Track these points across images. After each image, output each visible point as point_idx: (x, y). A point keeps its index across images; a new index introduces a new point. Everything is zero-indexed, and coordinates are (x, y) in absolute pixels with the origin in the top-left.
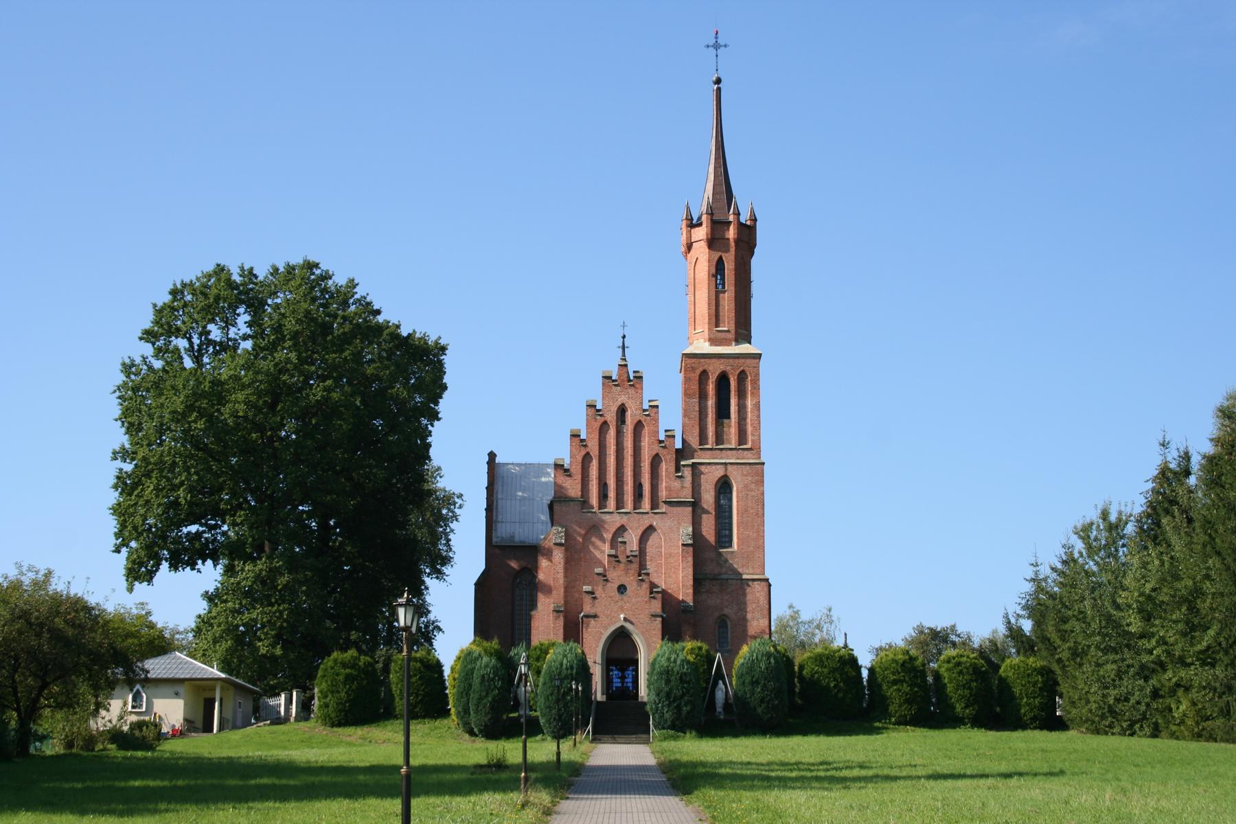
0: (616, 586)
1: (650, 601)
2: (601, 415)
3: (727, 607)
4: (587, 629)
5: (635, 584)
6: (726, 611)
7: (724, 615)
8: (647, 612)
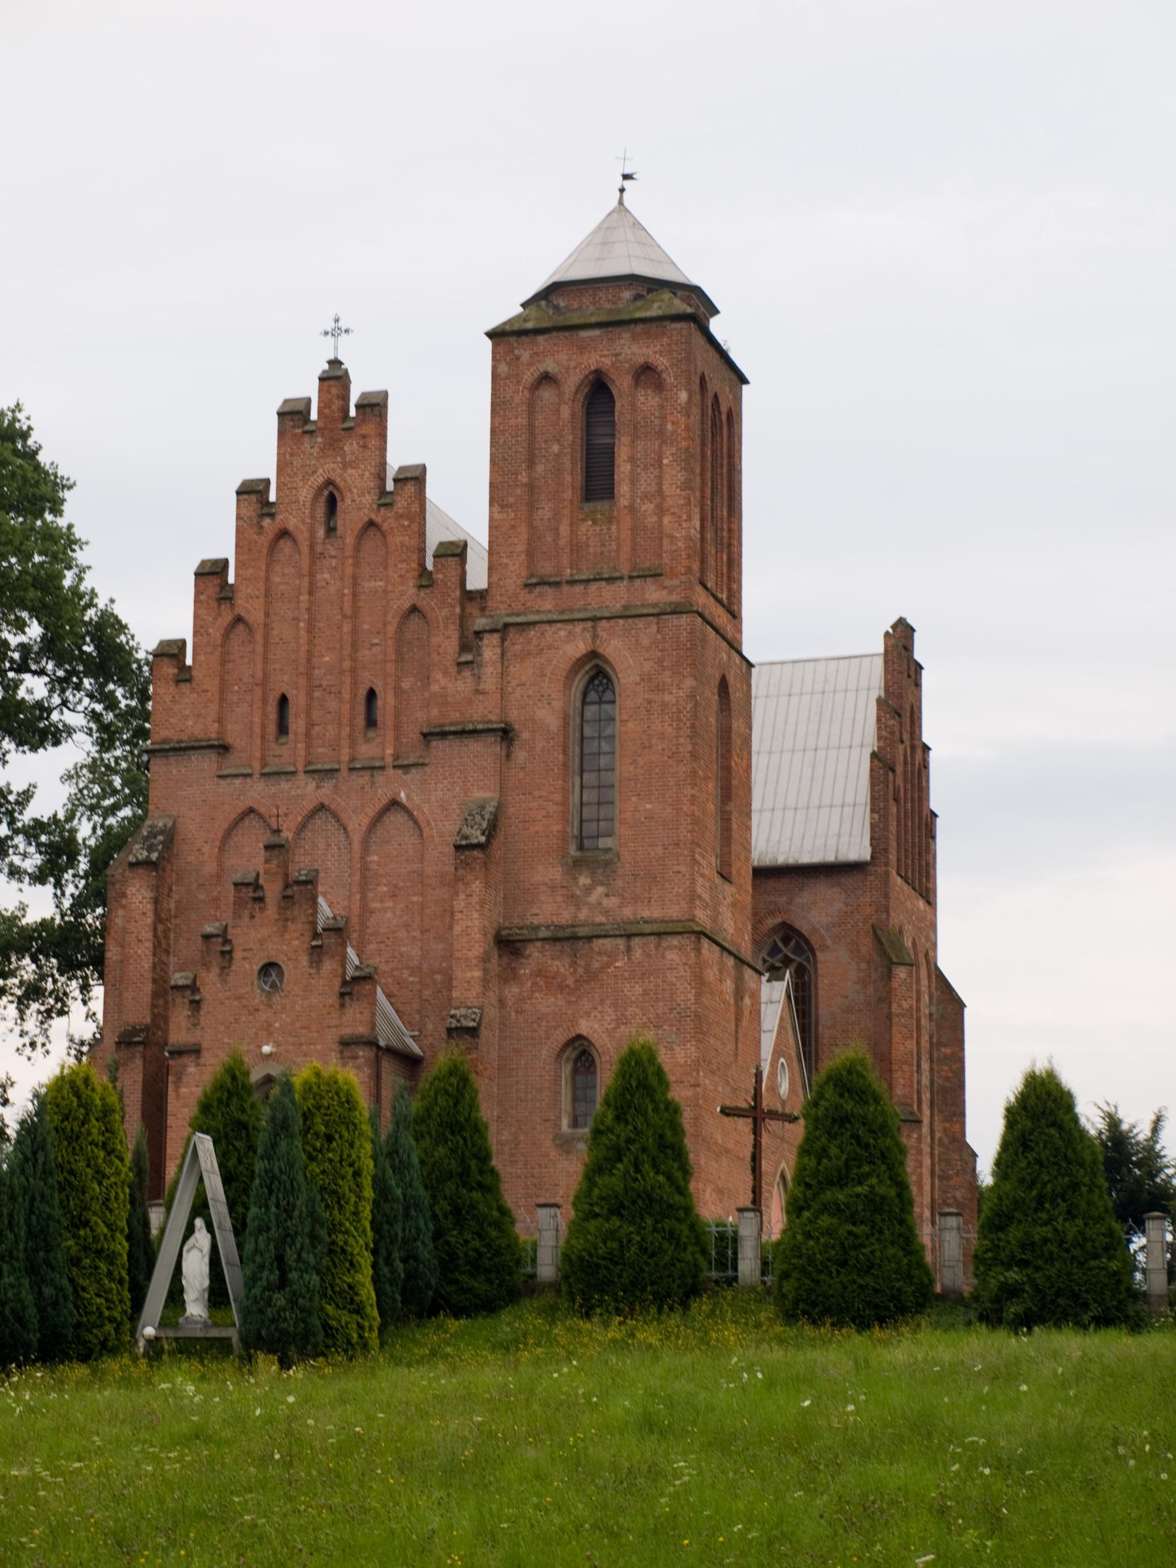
0: (256, 968)
1: (342, 1006)
2: (272, 516)
3: (588, 1014)
4: (177, 1087)
5: (304, 960)
6: (585, 1027)
7: (579, 1037)
8: (332, 1036)
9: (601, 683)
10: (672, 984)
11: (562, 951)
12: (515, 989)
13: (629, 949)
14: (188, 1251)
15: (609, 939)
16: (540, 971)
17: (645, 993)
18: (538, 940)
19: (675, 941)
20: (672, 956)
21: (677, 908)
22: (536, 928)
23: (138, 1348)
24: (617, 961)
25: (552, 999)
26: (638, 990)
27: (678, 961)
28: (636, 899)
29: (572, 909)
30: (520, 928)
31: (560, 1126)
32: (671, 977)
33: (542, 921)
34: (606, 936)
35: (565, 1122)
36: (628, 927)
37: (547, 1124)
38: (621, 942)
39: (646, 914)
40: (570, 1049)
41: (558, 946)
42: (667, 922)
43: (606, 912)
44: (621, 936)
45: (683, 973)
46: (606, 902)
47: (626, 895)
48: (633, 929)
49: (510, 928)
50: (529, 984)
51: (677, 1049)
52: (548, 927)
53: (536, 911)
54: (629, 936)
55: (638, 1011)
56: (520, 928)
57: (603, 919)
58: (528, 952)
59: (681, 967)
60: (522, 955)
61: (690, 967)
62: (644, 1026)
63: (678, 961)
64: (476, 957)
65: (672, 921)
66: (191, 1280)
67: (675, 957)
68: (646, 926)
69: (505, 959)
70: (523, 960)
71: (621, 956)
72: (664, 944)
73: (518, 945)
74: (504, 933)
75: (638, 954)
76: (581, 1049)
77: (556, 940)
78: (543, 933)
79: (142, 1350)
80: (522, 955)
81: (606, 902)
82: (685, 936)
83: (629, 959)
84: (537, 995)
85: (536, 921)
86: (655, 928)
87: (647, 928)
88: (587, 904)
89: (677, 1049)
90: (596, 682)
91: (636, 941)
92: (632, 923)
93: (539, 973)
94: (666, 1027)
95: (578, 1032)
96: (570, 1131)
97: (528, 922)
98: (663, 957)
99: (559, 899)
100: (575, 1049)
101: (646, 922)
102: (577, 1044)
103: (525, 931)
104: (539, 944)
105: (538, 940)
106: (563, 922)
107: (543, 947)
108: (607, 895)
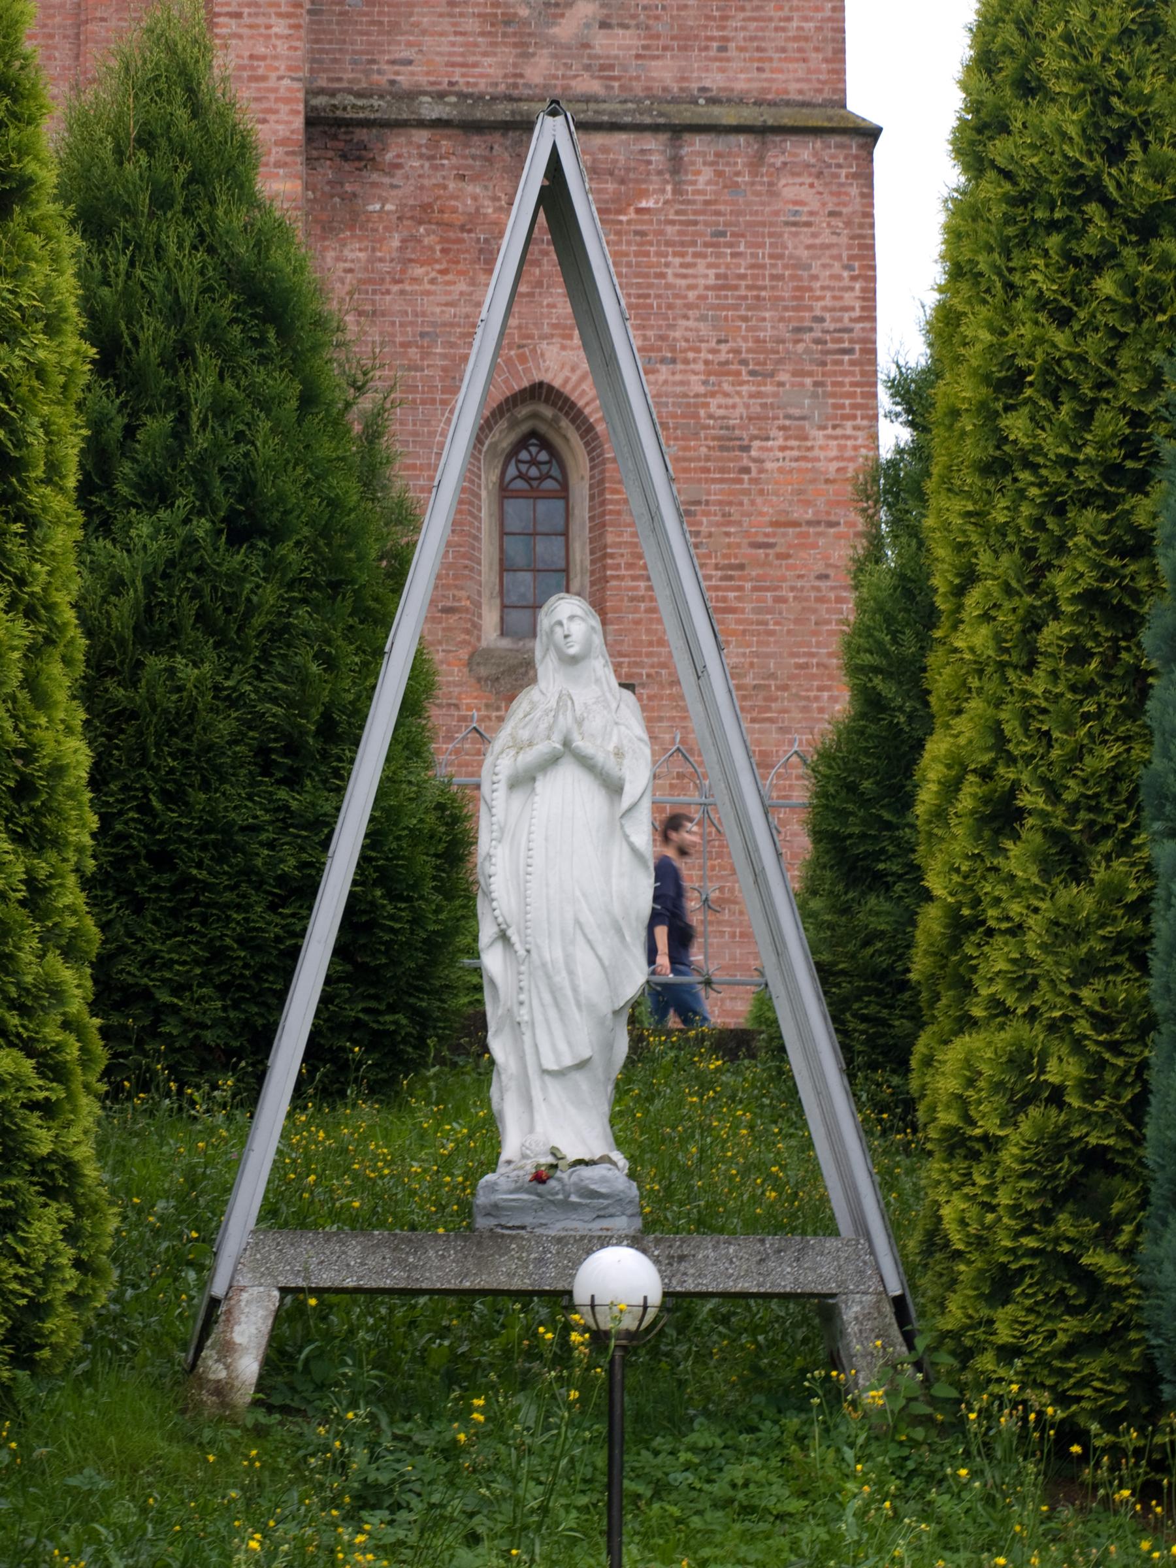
7: (540, 392)
9: (533, 462)
10: (799, 265)
11: (489, 160)
12: (355, 253)
13: (676, 165)
14: (524, 781)
15: (623, 136)
16: (426, 207)
17: (724, 284)
18: (421, 124)
19: (805, 151)
20: (793, 189)
21: (800, 69)
22: (412, 95)
23: (227, 1349)
24: (644, 194)
25: (462, 286)
26: (705, 274)
27: (815, 205)
28: (685, 41)
29: (507, 54)
30: (359, 95)
31: (477, 627)
32: (796, 245)
33: (423, 80)
34: (614, 127)
35: (490, 619)
36: (670, 108)
37: (453, 619)
38: (654, 144)
39: (714, 80)
40: (503, 424)
41: (478, 144)
42: (772, 104)
43: (604, 69)
44: (655, 128)
45: (826, 238)
46: (602, 42)
47: (659, 27)
48: (687, 115)
49: (333, 94)
50: (396, 243)
51: (818, 437)
52: (440, 96)
53: (405, 54)
54: (678, 131)
55: (704, 329)
56: (359, 95)
57: (595, 87)
58: (389, 156)
59: (822, 221)
60: (373, 164)
61: (848, 224)
62: (723, 369)
63: (815, 205)
64: (280, 143)
65: (788, 103)
66: (551, 952)
67: (805, 193)
68: (716, 110)
69: (327, 171)
70: (375, 177)
71: (654, 183)
72: (775, 158)
73: (362, 134)
74: (320, 101)
75: (702, 179)
76: (525, 428)
77: (472, 127)
78: (430, 110)
79: (249, 1367)
80: (373, 164)
81: (602, 42)
82: (834, 140)
83: (677, 191)
84: (419, 271)
85: (405, 79)
86: (748, 115)
87: (727, 116)
88: (550, 42)
89: (818, 437)
90: (524, 455)
91: (696, 145)
92: (675, 101)
93: (424, 213)
94: (783, 377)
95: (537, 377)
96: (505, 643)
97: (383, 80)
98: (773, 192)
99: (471, 25)
100: (514, 424)
101: (713, 101)
102: (523, 411)
103: (375, 102)
104: (422, 136)
105: (421, 124)
106: (482, 86)
107: (433, 144)
108: (604, 25)
